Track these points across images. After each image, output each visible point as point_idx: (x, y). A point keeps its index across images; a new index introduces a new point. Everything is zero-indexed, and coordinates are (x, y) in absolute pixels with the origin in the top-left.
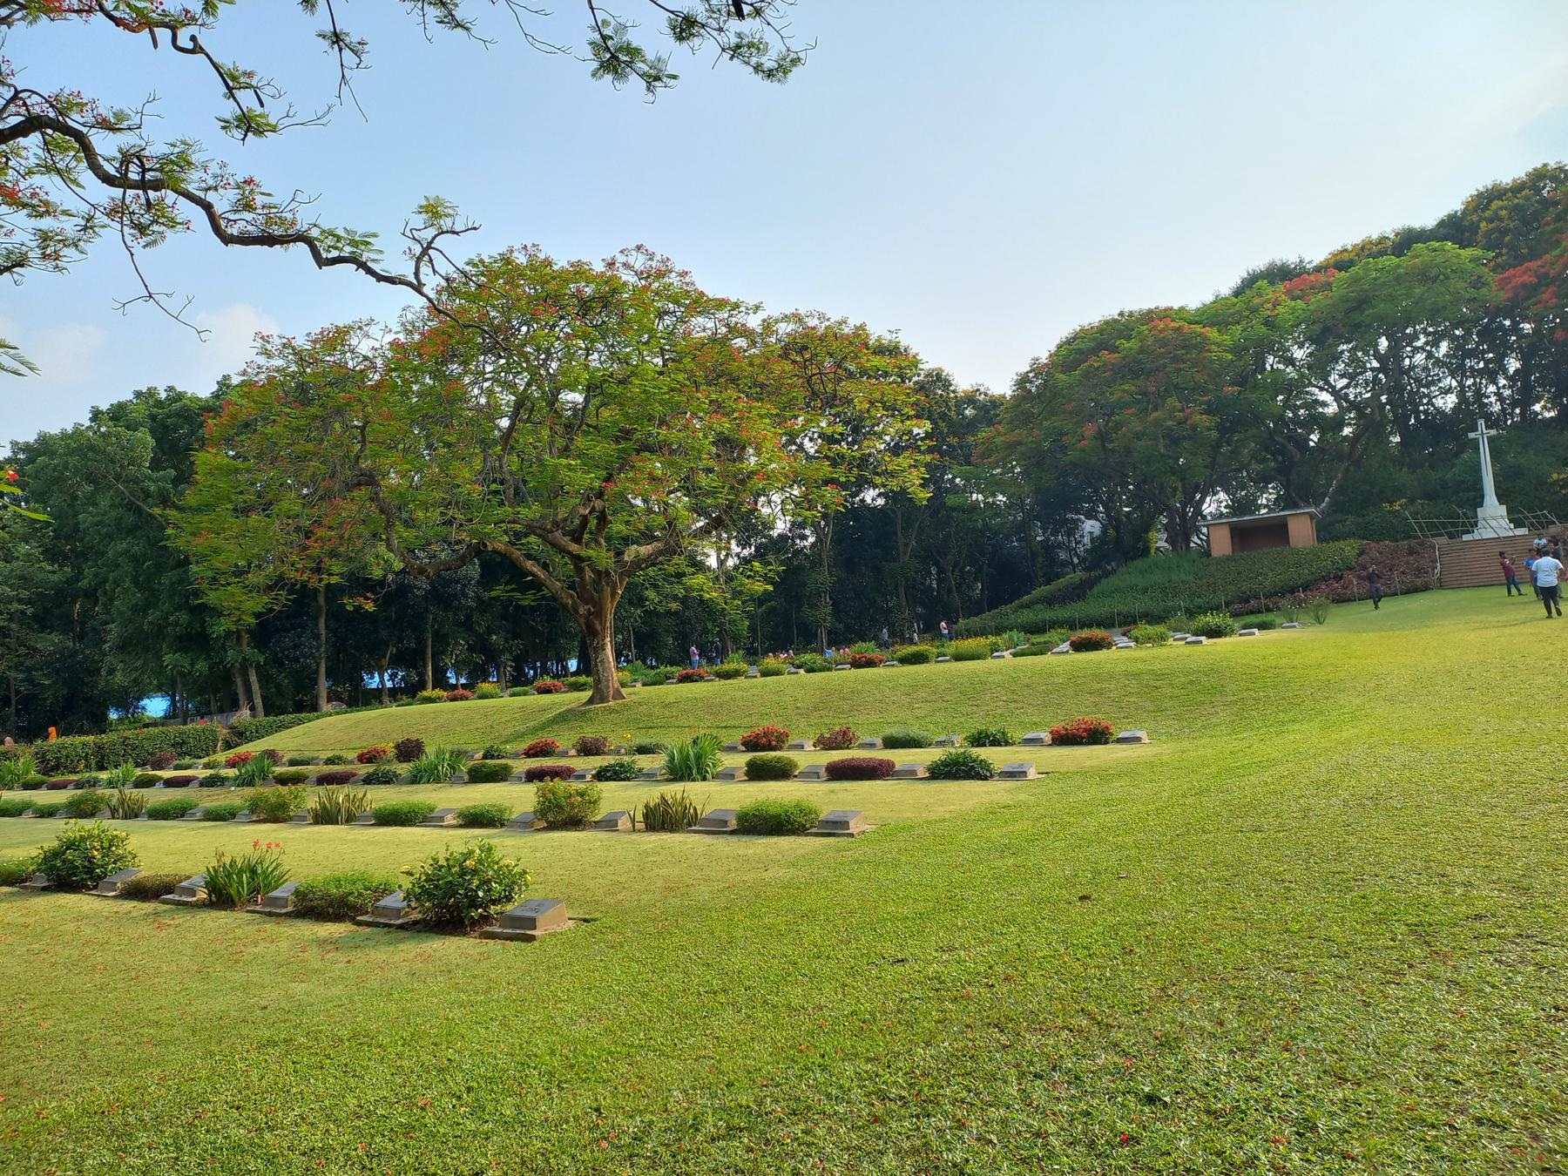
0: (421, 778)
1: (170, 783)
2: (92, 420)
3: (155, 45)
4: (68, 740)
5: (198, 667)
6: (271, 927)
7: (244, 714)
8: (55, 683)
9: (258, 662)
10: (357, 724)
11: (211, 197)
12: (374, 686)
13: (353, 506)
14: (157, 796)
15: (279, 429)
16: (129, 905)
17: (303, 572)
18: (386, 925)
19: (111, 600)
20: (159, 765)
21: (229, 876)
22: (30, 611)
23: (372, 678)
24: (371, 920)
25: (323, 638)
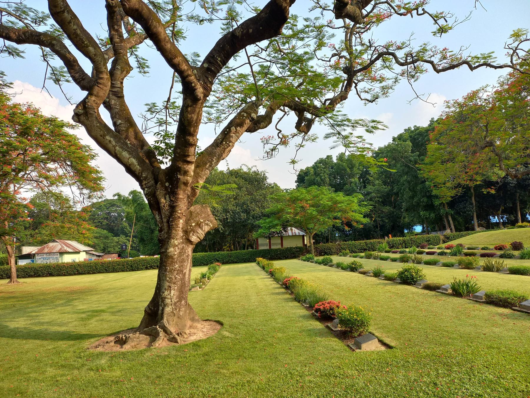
0: (525, 257)
1: (428, 253)
2: (393, 141)
3: (412, 17)
4: (395, 239)
5: (431, 215)
6: (478, 306)
7: (448, 232)
8: (389, 221)
9: (451, 214)
10: (491, 235)
11: (432, 59)
12: (495, 221)
13: (484, 154)
14: (426, 258)
15: (454, 132)
16: (426, 292)
17: (467, 181)
18: (526, 312)
19: (403, 195)
20: (423, 247)
21: (459, 286)
22: (381, 200)
23: (495, 218)
24: (519, 309)
25: (474, 204)
